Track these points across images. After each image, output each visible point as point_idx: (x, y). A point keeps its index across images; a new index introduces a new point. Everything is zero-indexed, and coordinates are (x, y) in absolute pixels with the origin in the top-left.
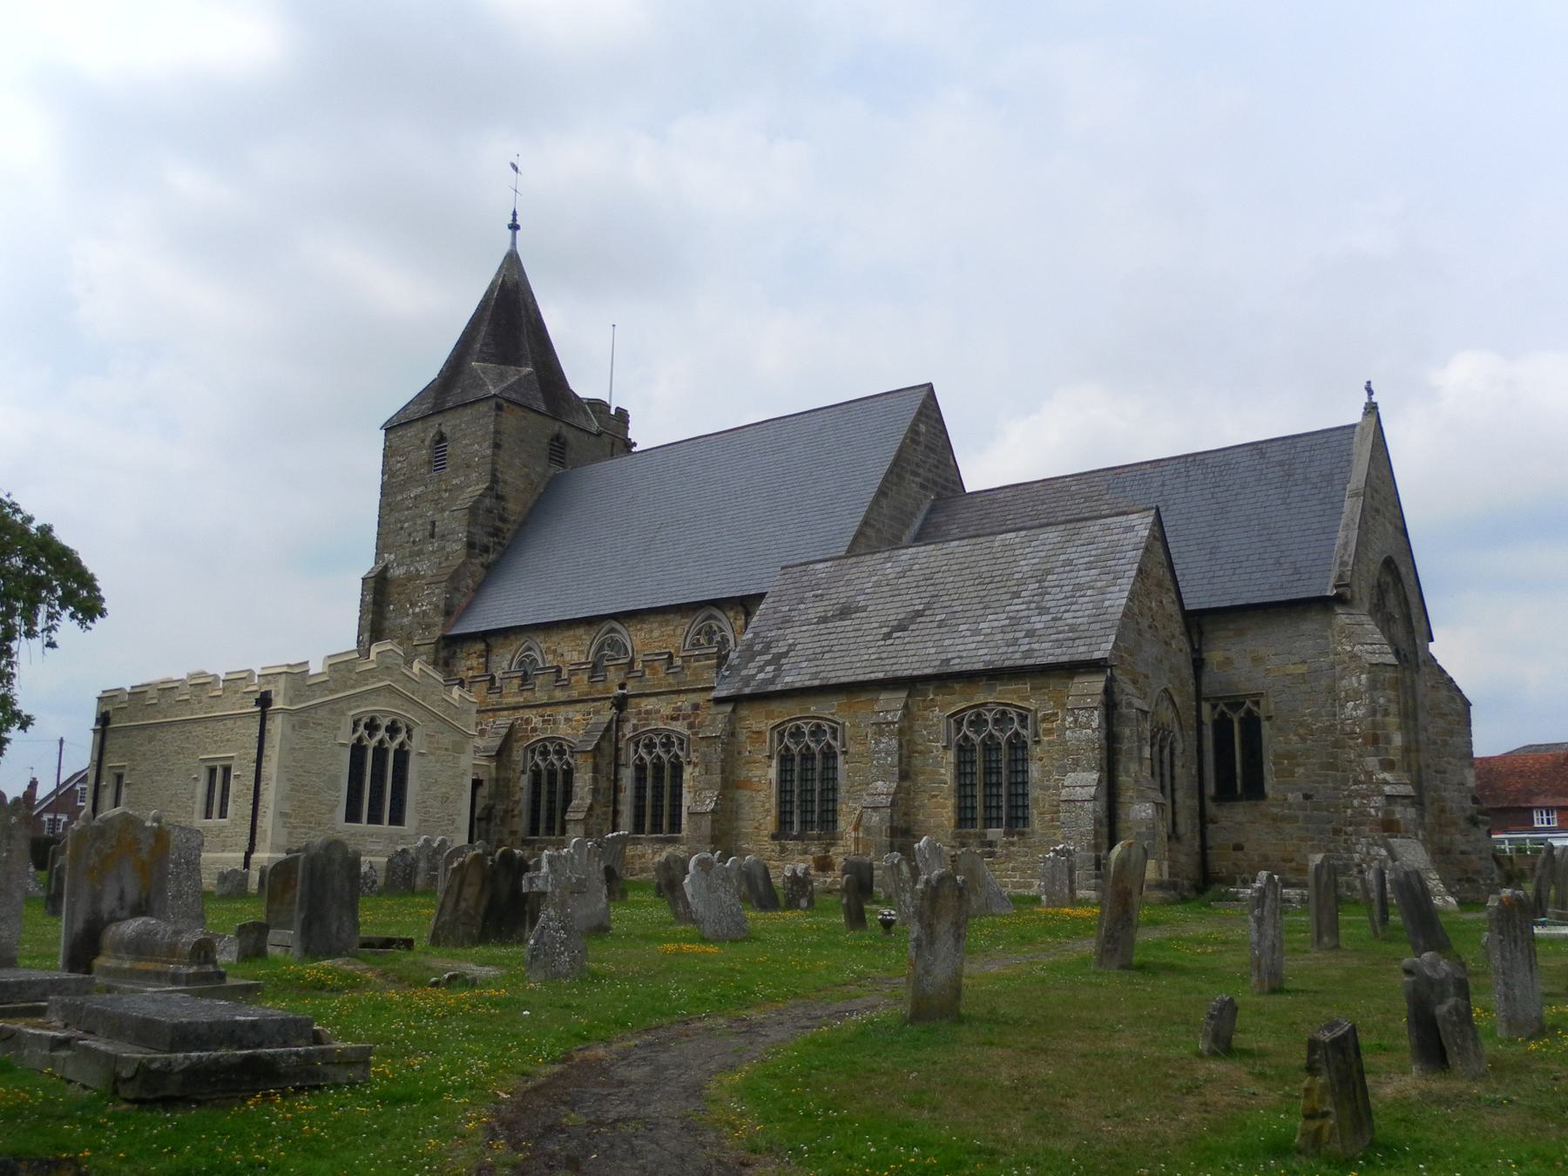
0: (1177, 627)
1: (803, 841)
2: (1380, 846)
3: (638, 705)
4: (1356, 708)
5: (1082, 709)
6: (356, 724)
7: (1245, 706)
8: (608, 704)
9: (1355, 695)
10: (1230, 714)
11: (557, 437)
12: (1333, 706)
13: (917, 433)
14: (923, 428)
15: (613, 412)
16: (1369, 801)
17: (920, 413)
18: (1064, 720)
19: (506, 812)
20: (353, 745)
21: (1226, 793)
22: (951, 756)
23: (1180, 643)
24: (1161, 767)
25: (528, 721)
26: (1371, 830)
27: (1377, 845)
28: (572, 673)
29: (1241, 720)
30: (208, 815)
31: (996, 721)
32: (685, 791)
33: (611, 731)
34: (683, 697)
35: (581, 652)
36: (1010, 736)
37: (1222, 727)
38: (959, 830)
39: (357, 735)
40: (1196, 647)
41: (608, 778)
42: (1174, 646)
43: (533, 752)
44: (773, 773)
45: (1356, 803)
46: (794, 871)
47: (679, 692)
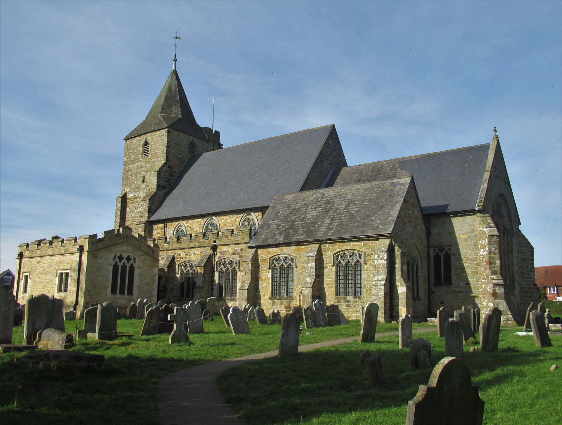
0: (420, 220)
1: (281, 300)
2: (491, 302)
3: (221, 249)
4: (484, 252)
5: (381, 252)
6: (115, 257)
7: (445, 250)
8: (209, 248)
9: (483, 246)
10: (440, 253)
11: (192, 143)
12: (476, 250)
13: (328, 144)
14: (330, 142)
15: (214, 132)
16: (488, 286)
17: (329, 136)
18: (375, 256)
19: (171, 289)
20: (114, 265)
21: (438, 282)
22: (334, 269)
23: (422, 227)
24: (413, 273)
25: (180, 254)
26: (488, 297)
27: (490, 302)
28: (196, 236)
29: (444, 255)
30: (114, 291)
31: (351, 256)
32: (238, 281)
33: (211, 258)
34: (237, 246)
35: (200, 228)
36: (346, 262)
37: (437, 257)
38: (337, 296)
39: (115, 261)
40: (428, 228)
41: (209, 277)
42: (418, 228)
43: (181, 266)
44: (270, 275)
45: (483, 286)
46: (273, 311)
47: (236, 244)
